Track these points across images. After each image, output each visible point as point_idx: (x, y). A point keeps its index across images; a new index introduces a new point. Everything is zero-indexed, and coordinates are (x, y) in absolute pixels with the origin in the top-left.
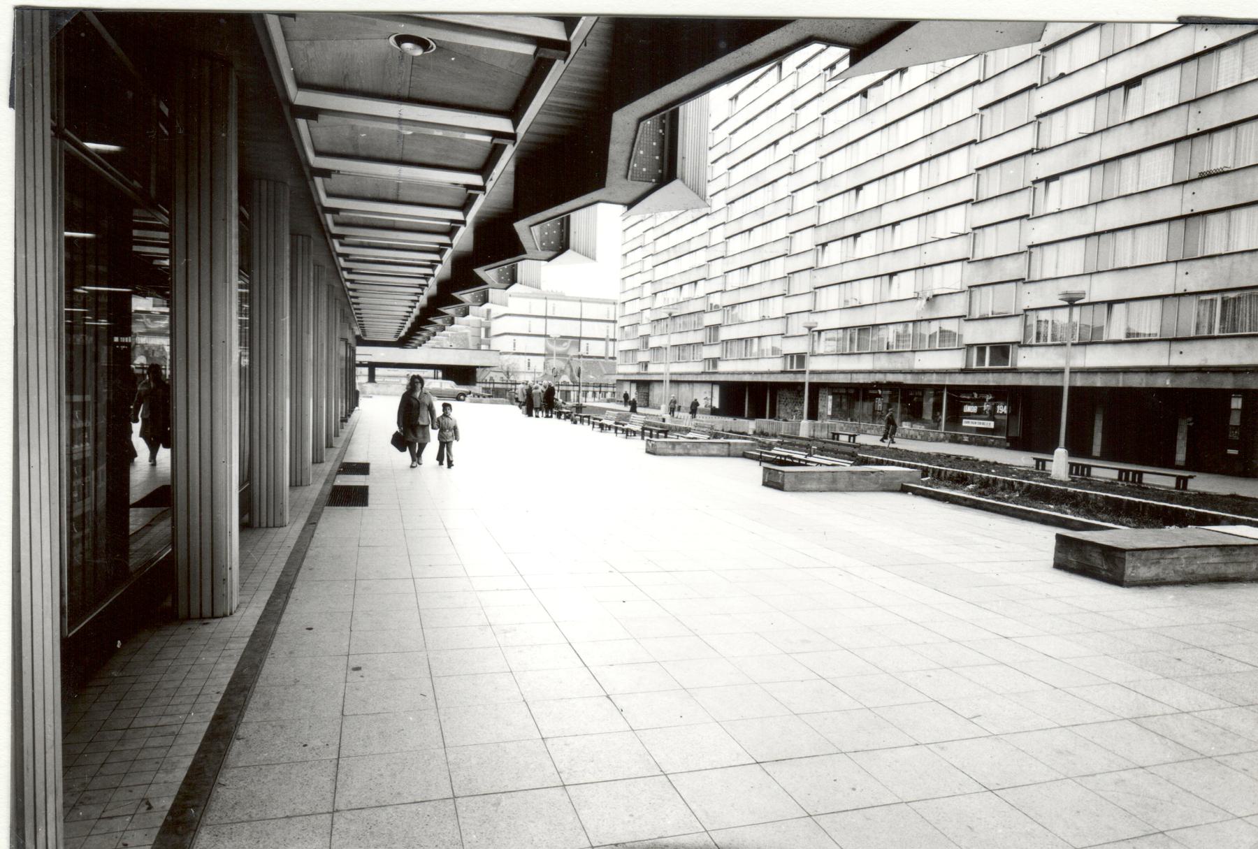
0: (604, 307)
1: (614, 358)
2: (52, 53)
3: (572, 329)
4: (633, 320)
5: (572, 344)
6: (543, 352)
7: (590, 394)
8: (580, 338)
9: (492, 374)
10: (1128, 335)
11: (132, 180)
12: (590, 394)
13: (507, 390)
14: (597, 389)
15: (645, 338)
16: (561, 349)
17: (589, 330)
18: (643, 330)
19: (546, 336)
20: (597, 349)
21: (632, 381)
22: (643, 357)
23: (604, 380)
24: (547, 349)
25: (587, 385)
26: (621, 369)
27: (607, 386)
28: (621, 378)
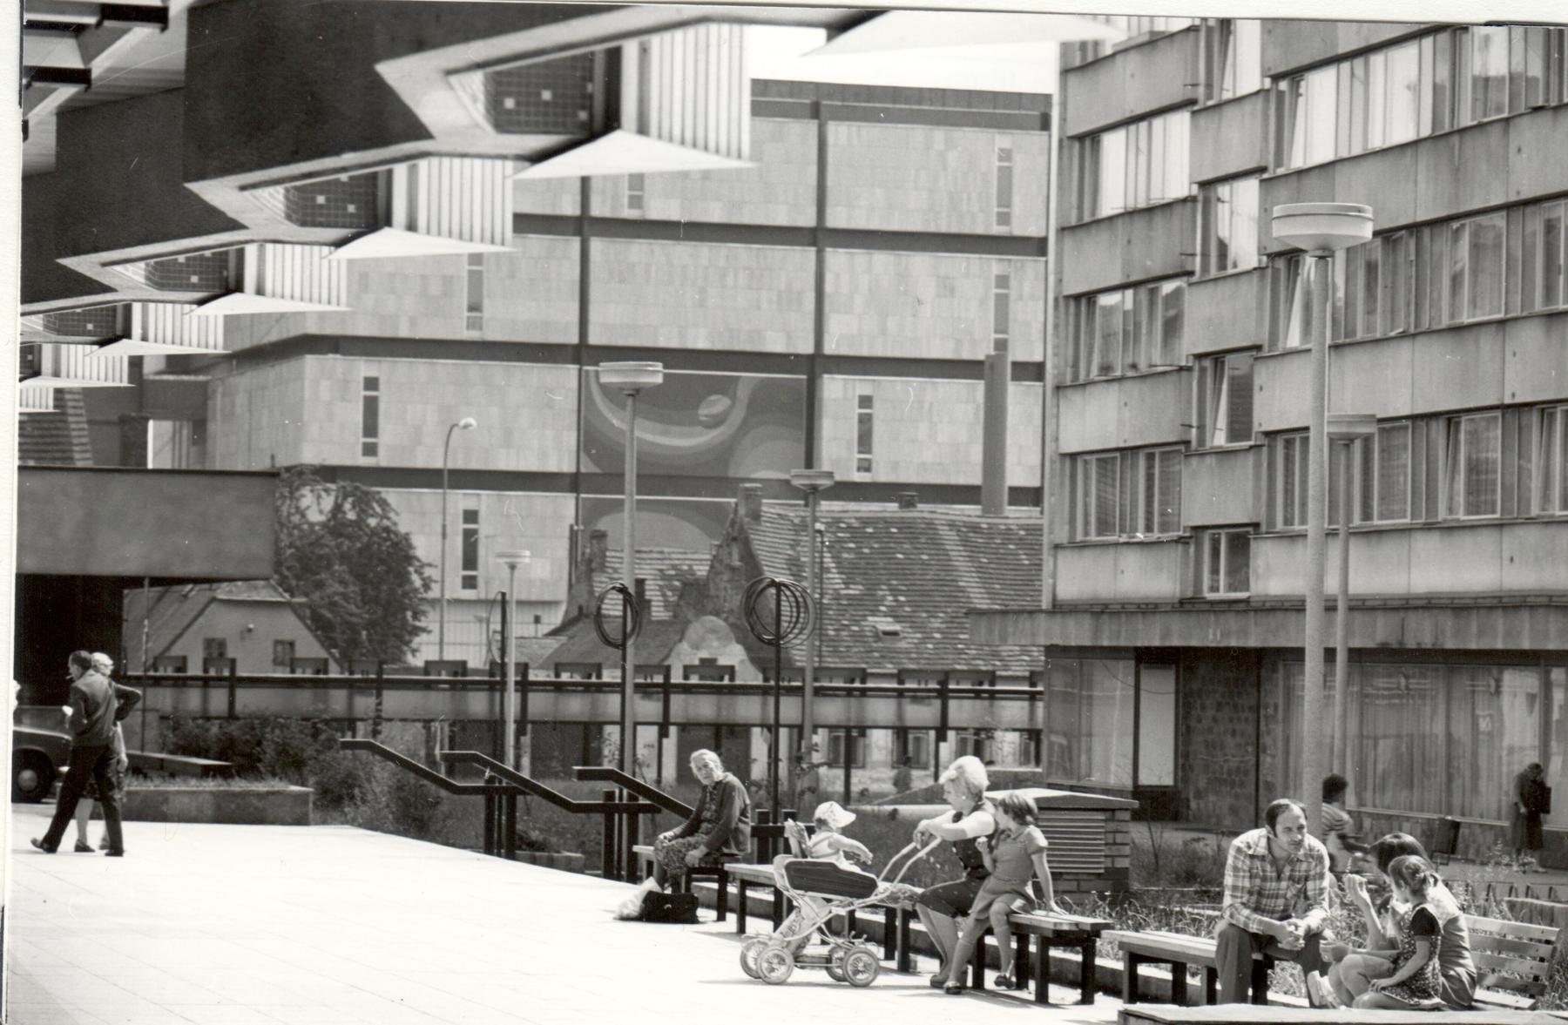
0: (982, 147)
1: (1030, 496)
2: (866, 499)
3: (750, 304)
4: (1154, 254)
5: (761, 406)
6: (563, 462)
7: (880, 743)
8: (816, 364)
9: (223, 623)
10: (1054, 606)
11: (188, 259)
12: (880, 743)
13: (315, 726)
14: (921, 714)
15: (1227, 370)
16: (680, 441)
17: (872, 304)
18: (1211, 318)
19: (582, 353)
20: (930, 436)
21: (1148, 658)
22: (1214, 496)
23: (969, 655)
24: (590, 438)
25: (856, 686)
26: (1075, 578)
27: (985, 687)
28: (1077, 633)
